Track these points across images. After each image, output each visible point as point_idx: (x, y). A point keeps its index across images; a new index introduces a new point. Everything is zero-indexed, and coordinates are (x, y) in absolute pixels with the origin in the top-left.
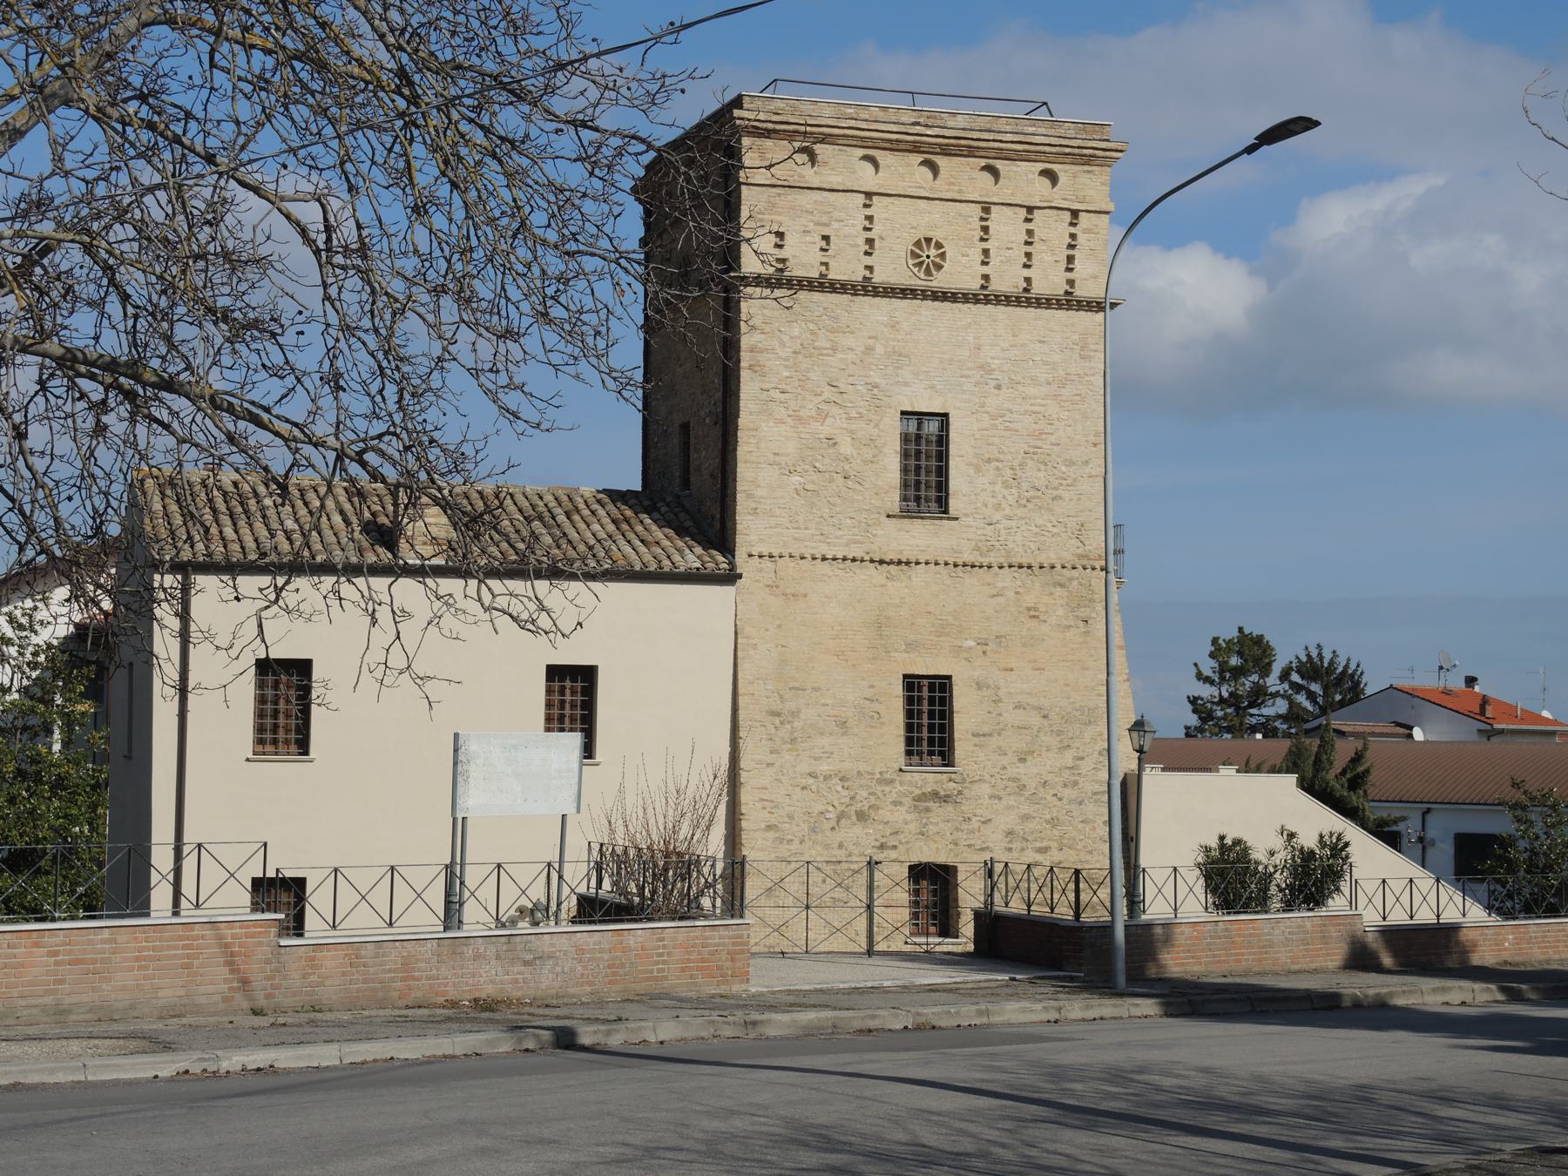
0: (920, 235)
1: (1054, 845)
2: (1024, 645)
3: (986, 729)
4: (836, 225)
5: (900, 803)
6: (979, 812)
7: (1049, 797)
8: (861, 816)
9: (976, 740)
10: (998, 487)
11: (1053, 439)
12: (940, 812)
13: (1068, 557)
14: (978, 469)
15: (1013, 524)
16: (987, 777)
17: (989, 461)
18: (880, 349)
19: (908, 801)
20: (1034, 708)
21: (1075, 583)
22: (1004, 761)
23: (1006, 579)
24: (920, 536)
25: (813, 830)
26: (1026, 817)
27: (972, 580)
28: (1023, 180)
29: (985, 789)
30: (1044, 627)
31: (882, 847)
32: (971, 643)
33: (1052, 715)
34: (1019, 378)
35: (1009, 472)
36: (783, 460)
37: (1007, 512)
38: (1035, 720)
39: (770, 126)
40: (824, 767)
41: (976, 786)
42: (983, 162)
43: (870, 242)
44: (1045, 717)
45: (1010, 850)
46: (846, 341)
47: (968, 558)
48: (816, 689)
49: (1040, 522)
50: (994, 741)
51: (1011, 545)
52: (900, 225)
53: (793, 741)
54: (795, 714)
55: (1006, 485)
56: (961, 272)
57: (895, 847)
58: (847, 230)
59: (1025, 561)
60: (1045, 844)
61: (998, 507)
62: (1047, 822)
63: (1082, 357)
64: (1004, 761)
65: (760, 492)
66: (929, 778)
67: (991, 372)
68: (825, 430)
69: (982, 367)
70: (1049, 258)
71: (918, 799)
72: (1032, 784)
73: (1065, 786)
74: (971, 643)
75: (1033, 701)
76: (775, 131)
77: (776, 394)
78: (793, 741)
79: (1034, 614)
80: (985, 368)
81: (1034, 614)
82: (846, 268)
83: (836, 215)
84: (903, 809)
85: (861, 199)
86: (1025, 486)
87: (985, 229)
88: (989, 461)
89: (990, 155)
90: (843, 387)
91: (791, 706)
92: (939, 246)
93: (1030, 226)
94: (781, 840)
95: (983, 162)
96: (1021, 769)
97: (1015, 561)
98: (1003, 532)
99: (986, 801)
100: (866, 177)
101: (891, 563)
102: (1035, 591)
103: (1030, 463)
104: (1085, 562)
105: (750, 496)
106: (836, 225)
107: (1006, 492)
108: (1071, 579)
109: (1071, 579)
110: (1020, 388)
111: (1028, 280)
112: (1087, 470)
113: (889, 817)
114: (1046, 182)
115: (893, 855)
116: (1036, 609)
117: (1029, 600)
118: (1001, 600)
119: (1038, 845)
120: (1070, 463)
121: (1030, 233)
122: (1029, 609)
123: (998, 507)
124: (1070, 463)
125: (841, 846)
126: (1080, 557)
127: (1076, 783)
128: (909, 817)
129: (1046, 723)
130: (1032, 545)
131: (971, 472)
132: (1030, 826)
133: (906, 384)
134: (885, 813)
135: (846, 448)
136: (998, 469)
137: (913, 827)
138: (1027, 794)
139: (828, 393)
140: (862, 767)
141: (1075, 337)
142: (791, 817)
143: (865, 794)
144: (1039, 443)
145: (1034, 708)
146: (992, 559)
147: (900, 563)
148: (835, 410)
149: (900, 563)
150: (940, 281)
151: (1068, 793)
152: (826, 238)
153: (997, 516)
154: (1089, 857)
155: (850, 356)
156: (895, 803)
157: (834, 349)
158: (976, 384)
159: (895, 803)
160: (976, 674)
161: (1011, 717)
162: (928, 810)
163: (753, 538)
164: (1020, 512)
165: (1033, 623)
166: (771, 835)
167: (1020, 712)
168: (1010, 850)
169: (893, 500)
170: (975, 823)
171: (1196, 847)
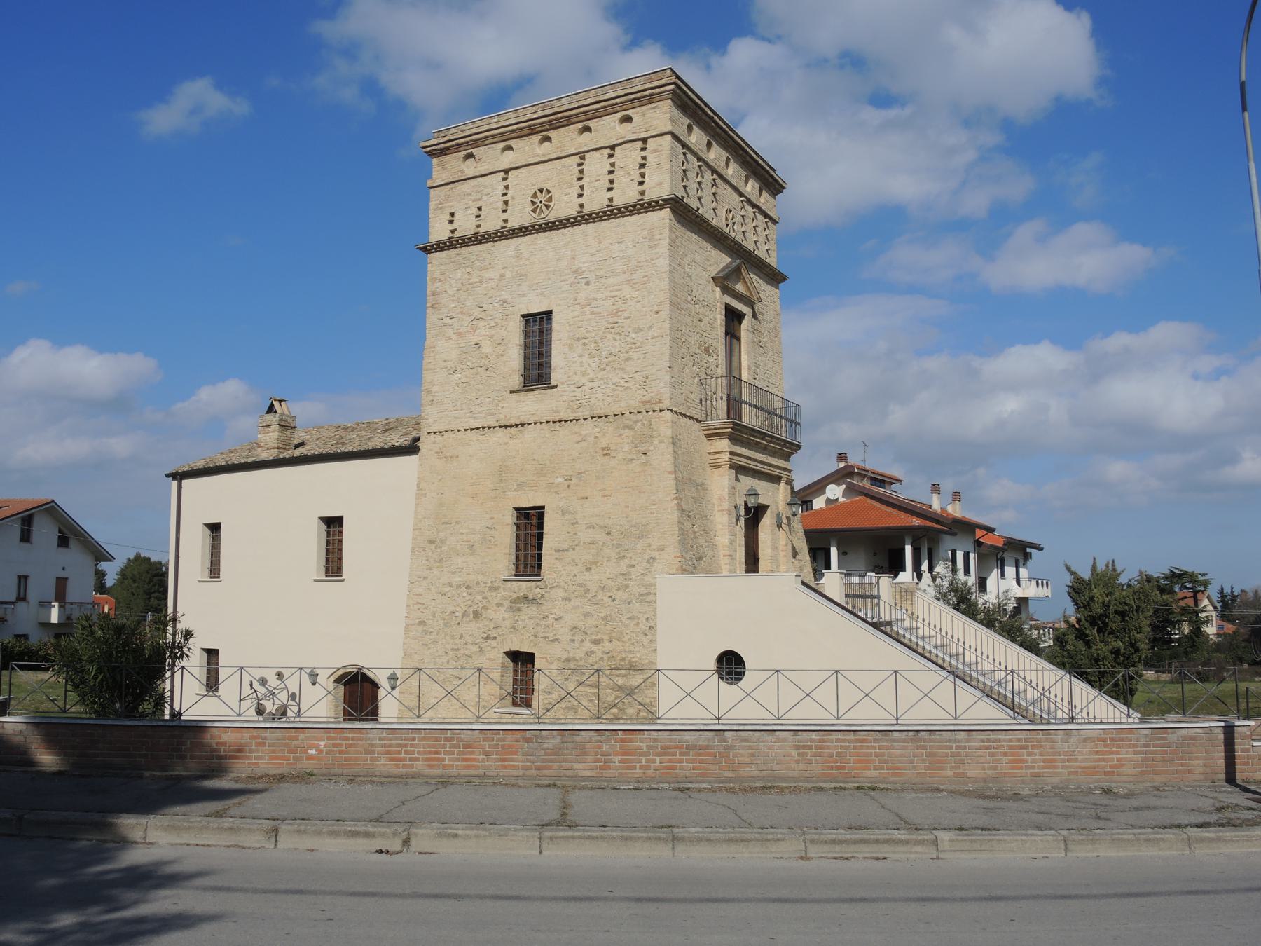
0: (536, 188)
1: (605, 637)
2: (598, 478)
3: (564, 546)
4: (485, 198)
5: (502, 605)
6: (554, 611)
7: (606, 599)
8: (477, 615)
9: (557, 555)
10: (586, 359)
11: (626, 314)
12: (529, 611)
13: (635, 404)
14: (571, 347)
15: (595, 384)
16: (562, 583)
17: (578, 339)
18: (508, 274)
19: (506, 603)
20: (601, 527)
21: (639, 424)
22: (575, 570)
23: (589, 428)
24: (534, 404)
25: (446, 625)
26: (587, 615)
27: (564, 432)
28: (608, 129)
29: (559, 593)
30: (613, 462)
31: (487, 638)
32: (560, 480)
33: (614, 532)
34: (602, 273)
35: (593, 345)
36: (449, 364)
37: (591, 376)
38: (600, 536)
39: (442, 146)
40: (457, 579)
41: (553, 591)
42: (580, 125)
43: (506, 203)
44: (609, 534)
45: (573, 641)
46: (490, 274)
47: (564, 416)
48: (457, 523)
49: (615, 379)
50: (569, 556)
51: (593, 401)
52: (524, 185)
53: (441, 560)
54: (443, 541)
55: (591, 356)
56: (564, 207)
57: (495, 638)
58: (492, 200)
59: (602, 412)
60: (599, 636)
61: (584, 374)
62: (603, 619)
63: (650, 247)
64: (575, 570)
65: (434, 389)
66: (524, 586)
67: (582, 273)
68: (474, 339)
69: (576, 271)
70: (625, 180)
71: (514, 602)
72: (593, 589)
73: (619, 589)
74: (560, 480)
75: (601, 522)
76: (447, 148)
77: (447, 321)
78: (441, 560)
79: (607, 453)
80: (578, 272)
81: (607, 453)
82: (491, 223)
83: (485, 191)
84: (502, 609)
85: (640, 144)
86: (604, 354)
87: (581, 172)
88: (578, 339)
89: (582, 118)
90: (486, 306)
91: (442, 535)
92: (535, 195)
93: (612, 160)
94: (426, 632)
95: (580, 125)
96: (587, 575)
97: (595, 413)
98: (588, 392)
99: (559, 603)
100: (508, 159)
101: (511, 426)
102: (608, 434)
103: (609, 336)
104: (648, 407)
105: (429, 392)
106: (485, 198)
107: (590, 361)
108: (636, 422)
109: (636, 422)
110: (603, 280)
111: (582, 206)
112: (650, 333)
113: (493, 616)
114: (587, 134)
115: (494, 643)
116: (608, 449)
117: (603, 442)
118: (584, 444)
119: (594, 637)
120: (639, 330)
121: (613, 165)
122: (603, 449)
123: (584, 374)
124: (639, 330)
125: (461, 636)
126: (645, 403)
127: (627, 586)
128: (506, 616)
129: (608, 538)
130: (609, 399)
131: (566, 349)
132: (590, 621)
133: (524, 295)
134: (490, 613)
135: (487, 348)
136: (584, 344)
137: (508, 623)
138: (589, 596)
139: (477, 313)
140: (480, 578)
141: (645, 233)
142: (434, 615)
143: (479, 598)
144: (615, 320)
145: (601, 527)
146: (580, 414)
147: (517, 426)
148: (482, 323)
149: (517, 426)
150: (552, 216)
151: (621, 595)
152: (480, 209)
153: (584, 380)
154: (632, 648)
155: (491, 284)
156: (499, 605)
157: (481, 282)
158: (573, 283)
159: (499, 605)
160: (562, 503)
161: (584, 535)
162: (519, 610)
163: (431, 420)
164: (600, 375)
165: (606, 459)
166: (420, 628)
167: (590, 531)
168: (573, 641)
169: (516, 380)
170: (550, 621)
171: (317, 520)
